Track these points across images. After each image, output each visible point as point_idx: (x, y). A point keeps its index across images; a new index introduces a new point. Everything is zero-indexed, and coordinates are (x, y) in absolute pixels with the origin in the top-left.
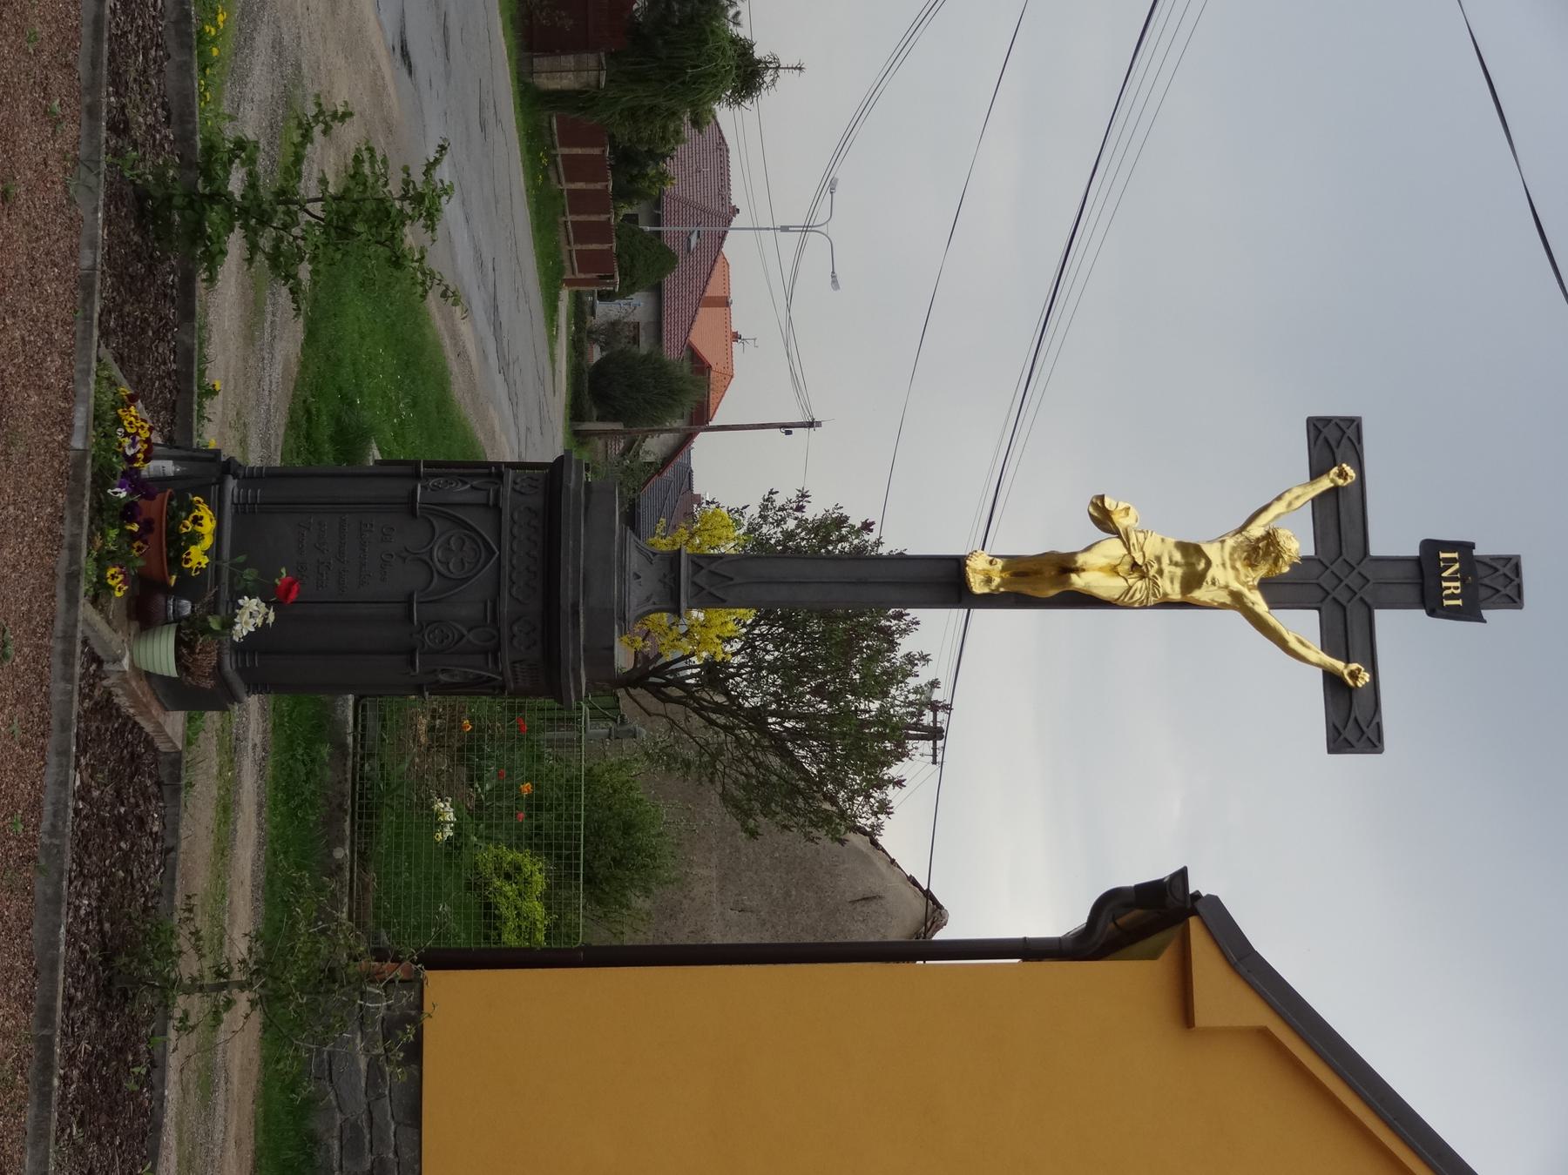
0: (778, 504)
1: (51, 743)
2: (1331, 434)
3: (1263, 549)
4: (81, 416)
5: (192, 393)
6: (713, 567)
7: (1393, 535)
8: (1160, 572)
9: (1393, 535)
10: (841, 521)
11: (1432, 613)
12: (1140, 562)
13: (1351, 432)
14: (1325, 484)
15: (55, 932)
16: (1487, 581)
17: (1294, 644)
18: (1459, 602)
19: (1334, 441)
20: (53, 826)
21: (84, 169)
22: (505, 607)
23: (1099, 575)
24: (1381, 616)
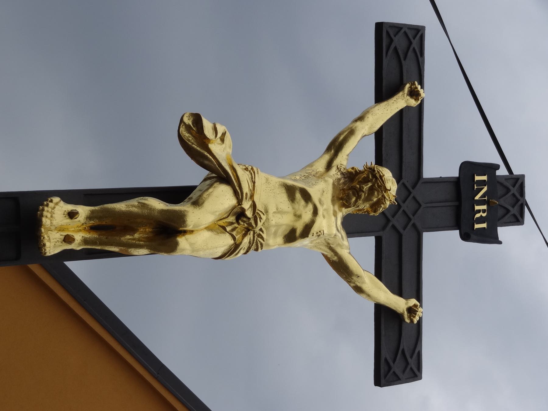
7: (440, 163)
9: (440, 163)
11: (465, 237)
18: (484, 225)
23: (207, 234)
24: (428, 238)
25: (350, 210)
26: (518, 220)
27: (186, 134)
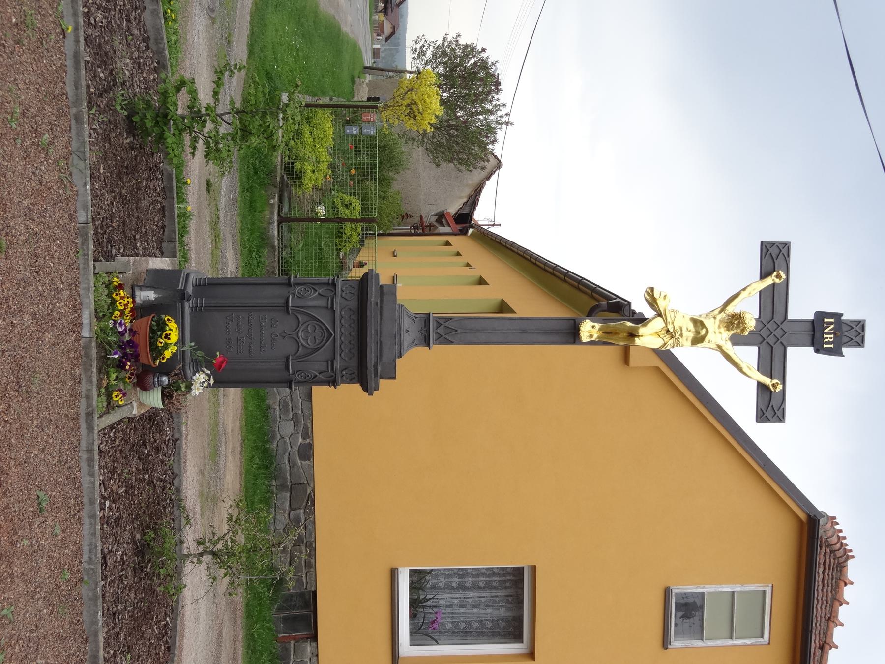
0: (449, 40)
1: (84, 514)
2: (774, 251)
3: (735, 321)
4: (86, 316)
5: (173, 198)
6: (447, 324)
7: (800, 309)
8: (681, 335)
9: (800, 309)
10: (473, 49)
11: (817, 351)
12: (671, 330)
13: (784, 251)
14: (769, 281)
15: (96, 617)
16: (846, 334)
17: (745, 370)
18: (832, 346)
19: (774, 257)
20: (90, 558)
21: (75, 157)
22: (338, 365)
24: (790, 350)
25: (732, 332)
26: (860, 343)
27: (648, 297)
